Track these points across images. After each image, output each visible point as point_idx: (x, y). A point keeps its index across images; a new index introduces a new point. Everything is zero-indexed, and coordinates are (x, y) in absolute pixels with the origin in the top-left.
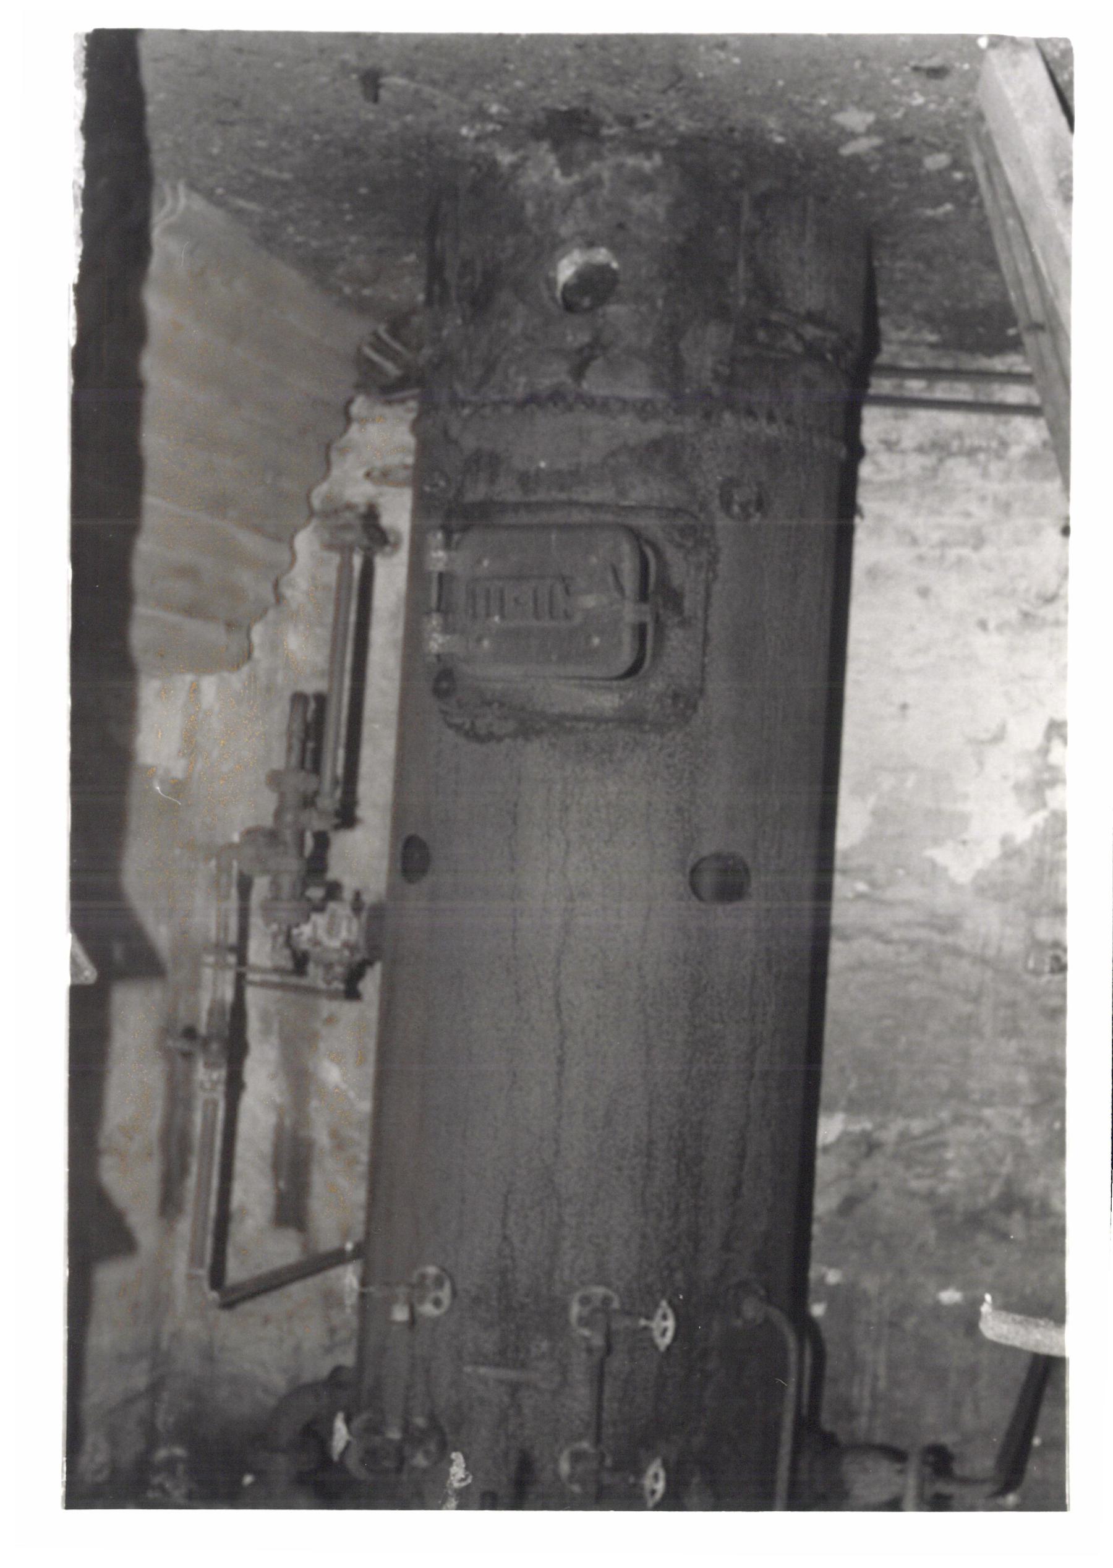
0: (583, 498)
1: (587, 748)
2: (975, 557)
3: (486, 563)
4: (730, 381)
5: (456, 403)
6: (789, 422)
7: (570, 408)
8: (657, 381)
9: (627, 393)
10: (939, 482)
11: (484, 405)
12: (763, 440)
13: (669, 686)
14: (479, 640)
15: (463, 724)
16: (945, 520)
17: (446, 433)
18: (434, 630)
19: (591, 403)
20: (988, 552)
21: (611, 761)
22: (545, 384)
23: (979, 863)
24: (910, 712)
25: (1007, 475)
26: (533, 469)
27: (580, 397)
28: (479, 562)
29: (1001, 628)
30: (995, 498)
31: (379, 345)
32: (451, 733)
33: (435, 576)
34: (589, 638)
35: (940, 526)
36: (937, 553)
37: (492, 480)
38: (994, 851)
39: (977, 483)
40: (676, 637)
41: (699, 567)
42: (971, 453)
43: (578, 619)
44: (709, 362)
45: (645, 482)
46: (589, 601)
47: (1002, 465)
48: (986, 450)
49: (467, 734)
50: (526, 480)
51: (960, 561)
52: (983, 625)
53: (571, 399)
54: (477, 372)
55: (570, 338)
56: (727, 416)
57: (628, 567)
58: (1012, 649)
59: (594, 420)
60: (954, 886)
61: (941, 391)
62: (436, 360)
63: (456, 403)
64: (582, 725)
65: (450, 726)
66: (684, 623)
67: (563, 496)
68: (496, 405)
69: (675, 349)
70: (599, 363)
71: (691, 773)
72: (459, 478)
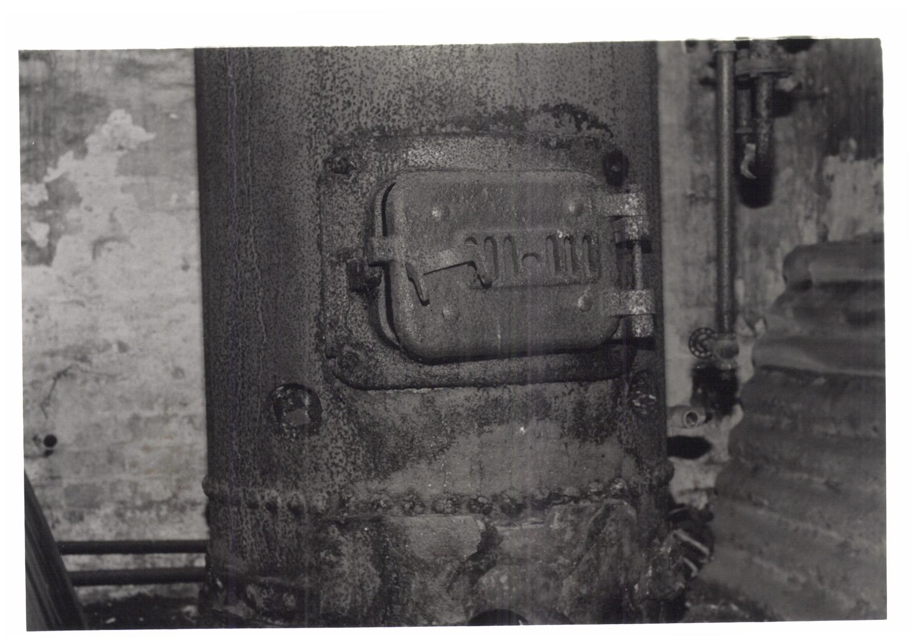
0: (469, 392)
1: (440, 101)
2: (136, 409)
3: (580, 303)
4: (318, 544)
5: (631, 495)
6: (253, 506)
7: (495, 498)
8: (399, 534)
9: (431, 519)
10: (175, 477)
11: (598, 494)
12: (279, 484)
13: (355, 181)
14: (580, 211)
15: (589, 128)
16: (165, 442)
17: (639, 462)
18: (635, 218)
19: (477, 507)
20: (125, 415)
21: (411, 89)
22: (529, 523)
23: (105, 130)
24: (180, 262)
25: (114, 487)
26: (533, 421)
27: (486, 511)
28: (588, 303)
29: (108, 346)
30: (123, 465)
31: (696, 555)
32: (603, 119)
33: (639, 284)
34: (446, 214)
35: (170, 437)
36: (170, 411)
37: (581, 406)
38: (92, 141)
39: (142, 479)
40: (351, 239)
41: (334, 324)
42: (149, 505)
43: (460, 236)
44: (346, 564)
45: (404, 419)
46: (447, 258)
47: (119, 496)
48: (134, 508)
49: (585, 116)
50: (544, 410)
51: (150, 405)
52: (123, 347)
53: (496, 507)
54: (610, 529)
55: (504, 579)
56: (321, 505)
57: (406, 305)
58: (93, 328)
59: (468, 487)
60: (125, 105)
61: (181, 560)
62: (656, 541)
63: (631, 495)
64: (449, 128)
65: (605, 127)
66: (344, 255)
67: (494, 393)
68: (584, 495)
69: (384, 577)
70: (468, 552)
71: (324, 88)
72: (619, 409)
